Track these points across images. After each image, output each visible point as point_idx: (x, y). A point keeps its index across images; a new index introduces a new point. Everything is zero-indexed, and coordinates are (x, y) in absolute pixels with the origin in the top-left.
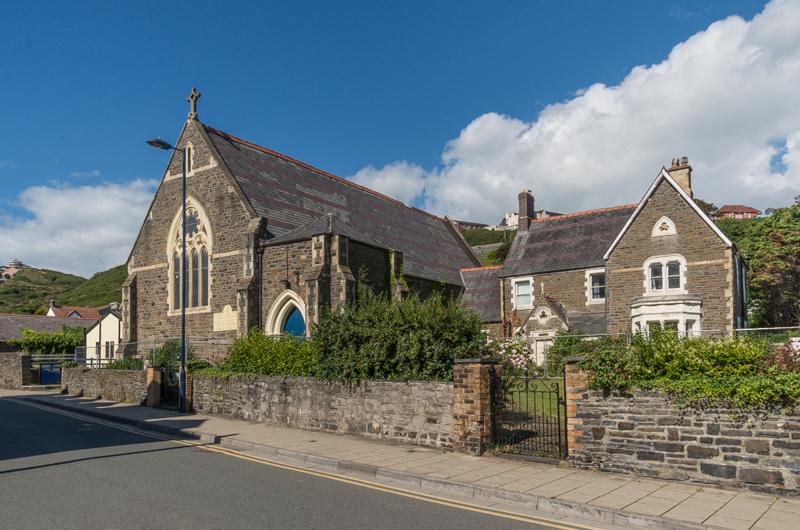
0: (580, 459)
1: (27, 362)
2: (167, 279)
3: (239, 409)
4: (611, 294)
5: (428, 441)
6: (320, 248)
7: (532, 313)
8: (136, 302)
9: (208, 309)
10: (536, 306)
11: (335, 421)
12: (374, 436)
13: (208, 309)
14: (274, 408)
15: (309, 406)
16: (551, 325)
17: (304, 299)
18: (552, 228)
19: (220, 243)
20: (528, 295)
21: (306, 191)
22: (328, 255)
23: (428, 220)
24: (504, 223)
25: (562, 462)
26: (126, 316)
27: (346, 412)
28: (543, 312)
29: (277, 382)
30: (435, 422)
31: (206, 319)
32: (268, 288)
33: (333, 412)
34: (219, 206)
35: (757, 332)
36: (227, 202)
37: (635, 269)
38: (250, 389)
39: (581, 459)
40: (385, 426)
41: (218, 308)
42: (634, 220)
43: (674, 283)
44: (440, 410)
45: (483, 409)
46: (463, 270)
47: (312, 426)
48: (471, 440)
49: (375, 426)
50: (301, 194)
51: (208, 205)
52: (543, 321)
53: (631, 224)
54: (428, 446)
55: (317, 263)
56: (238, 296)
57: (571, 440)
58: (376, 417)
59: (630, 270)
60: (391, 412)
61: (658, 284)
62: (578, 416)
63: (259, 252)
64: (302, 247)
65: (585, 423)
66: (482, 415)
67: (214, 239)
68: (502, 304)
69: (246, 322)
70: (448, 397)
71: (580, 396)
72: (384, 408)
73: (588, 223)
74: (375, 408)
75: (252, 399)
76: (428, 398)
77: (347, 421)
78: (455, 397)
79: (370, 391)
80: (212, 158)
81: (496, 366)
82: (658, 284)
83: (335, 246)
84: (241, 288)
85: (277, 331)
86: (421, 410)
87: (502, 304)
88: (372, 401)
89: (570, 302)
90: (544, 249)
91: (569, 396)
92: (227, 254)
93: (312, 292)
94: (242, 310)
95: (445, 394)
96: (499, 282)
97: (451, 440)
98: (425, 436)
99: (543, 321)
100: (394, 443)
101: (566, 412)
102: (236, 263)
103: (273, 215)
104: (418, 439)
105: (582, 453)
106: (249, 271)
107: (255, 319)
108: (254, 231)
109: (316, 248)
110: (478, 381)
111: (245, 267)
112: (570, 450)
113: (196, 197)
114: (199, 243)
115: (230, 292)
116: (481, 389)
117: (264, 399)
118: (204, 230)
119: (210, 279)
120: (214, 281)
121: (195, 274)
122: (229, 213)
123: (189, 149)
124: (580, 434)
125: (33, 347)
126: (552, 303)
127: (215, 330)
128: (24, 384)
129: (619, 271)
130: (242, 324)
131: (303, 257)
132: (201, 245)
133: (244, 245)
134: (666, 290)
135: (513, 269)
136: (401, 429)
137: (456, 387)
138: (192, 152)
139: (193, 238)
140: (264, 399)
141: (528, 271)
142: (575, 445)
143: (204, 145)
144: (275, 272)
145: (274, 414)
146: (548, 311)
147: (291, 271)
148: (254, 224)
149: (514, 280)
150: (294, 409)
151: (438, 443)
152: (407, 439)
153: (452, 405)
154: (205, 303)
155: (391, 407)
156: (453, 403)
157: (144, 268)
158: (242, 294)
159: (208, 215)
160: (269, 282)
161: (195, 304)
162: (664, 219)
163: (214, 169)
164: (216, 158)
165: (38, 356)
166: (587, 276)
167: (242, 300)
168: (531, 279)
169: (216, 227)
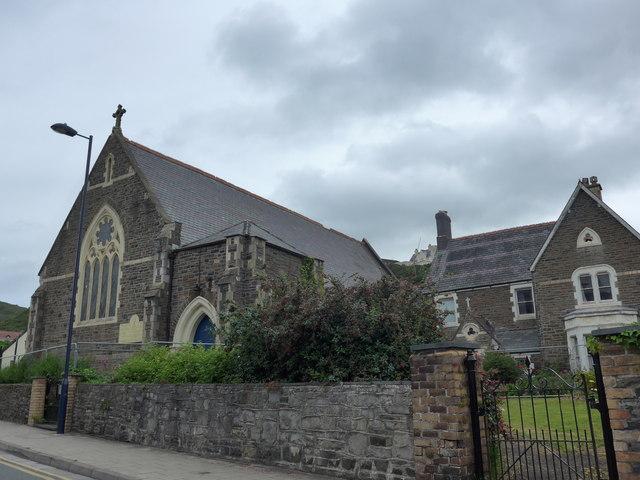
3: (123, 428)
6: (235, 250)
7: (459, 330)
10: (461, 322)
13: (115, 320)
15: (205, 422)
17: (215, 306)
18: (469, 247)
19: (132, 250)
26: (32, 327)
27: (253, 430)
28: (471, 329)
30: (382, 443)
31: (112, 330)
37: (564, 281)
41: (125, 318)
43: (606, 295)
44: (390, 424)
49: (294, 450)
51: (124, 213)
58: (294, 437)
59: (558, 281)
60: (316, 430)
61: (589, 296)
67: (126, 247)
72: (306, 424)
74: (294, 424)
77: (255, 445)
82: (589, 296)
86: (361, 426)
90: (466, 266)
91: (610, 393)
92: (138, 261)
94: (149, 319)
102: (147, 269)
106: (159, 278)
113: (113, 206)
118: (118, 237)
119: (119, 287)
120: (123, 290)
121: (105, 276)
122: (143, 219)
130: (148, 334)
131: (217, 261)
134: (598, 302)
137: (414, 387)
138: (113, 162)
140: (152, 414)
146: (476, 328)
150: (187, 428)
152: (341, 470)
154: (112, 313)
155: (317, 422)
157: (53, 279)
159: (122, 222)
161: (102, 314)
162: (587, 230)
166: (512, 291)
167: (150, 307)
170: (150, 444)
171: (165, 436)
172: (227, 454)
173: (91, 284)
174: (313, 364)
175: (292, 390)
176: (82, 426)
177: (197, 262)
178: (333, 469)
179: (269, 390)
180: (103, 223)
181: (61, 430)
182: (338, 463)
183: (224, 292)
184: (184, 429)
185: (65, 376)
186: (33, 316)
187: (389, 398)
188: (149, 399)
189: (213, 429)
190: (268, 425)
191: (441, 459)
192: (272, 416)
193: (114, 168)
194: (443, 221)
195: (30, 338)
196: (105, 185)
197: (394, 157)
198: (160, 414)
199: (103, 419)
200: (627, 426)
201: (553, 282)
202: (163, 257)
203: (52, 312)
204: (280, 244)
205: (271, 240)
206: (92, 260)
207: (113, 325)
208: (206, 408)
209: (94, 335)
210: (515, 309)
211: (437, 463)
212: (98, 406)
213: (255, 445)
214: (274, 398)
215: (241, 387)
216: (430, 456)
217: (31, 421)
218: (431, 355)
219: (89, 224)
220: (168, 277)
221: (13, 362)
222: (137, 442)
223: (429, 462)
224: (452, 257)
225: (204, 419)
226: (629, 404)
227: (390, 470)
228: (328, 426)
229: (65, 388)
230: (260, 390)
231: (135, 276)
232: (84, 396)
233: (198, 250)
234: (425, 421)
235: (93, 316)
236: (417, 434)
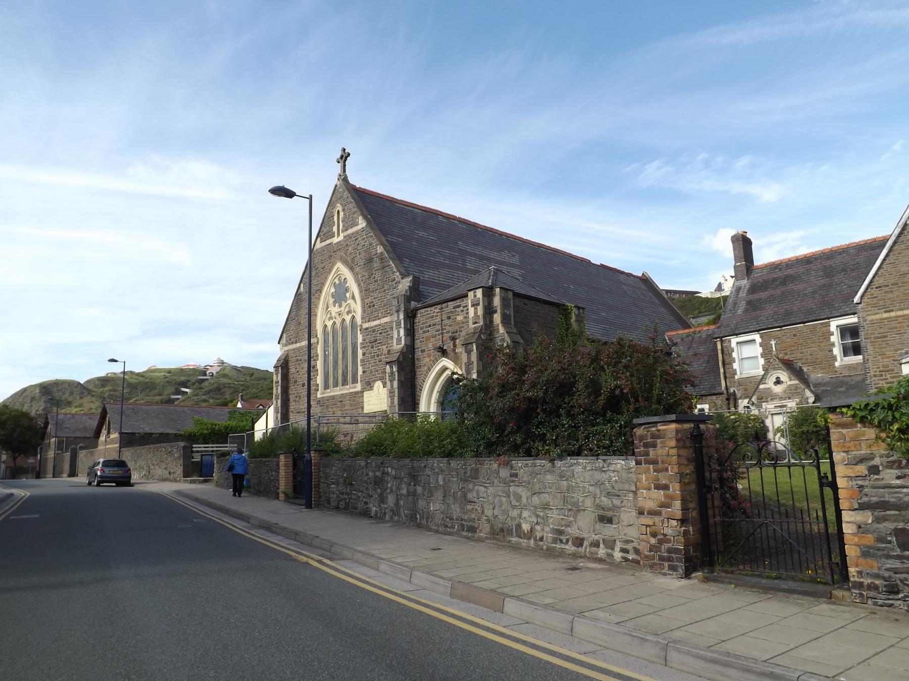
0: (873, 587)
1: (188, 453)
2: (317, 356)
3: (366, 503)
4: (870, 348)
5: (602, 552)
6: (478, 304)
7: (763, 379)
8: (288, 383)
9: (358, 387)
10: (766, 370)
11: (473, 520)
12: (524, 542)
13: (358, 387)
14: (402, 503)
16: (791, 393)
18: (778, 274)
19: (370, 310)
20: (757, 357)
22: (489, 311)
23: (622, 277)
24: (719, 288)
25: (838, 593)
26: (277, 399)
27: (486, 506)
29: (405, 466)
30: (610, 521)
31: (356, 399)
32: (423, 359)
33: (469, 507)
34: (367, 269)
36: (376, 264)
37: (900, 313)
38: (376, 477)
39: (876, 588)
40: (538, 528)
41: (369, 385)
42: (890, 250)
44: (617, 502)
45: (684, 501)
46: (669, 334)
47: (446, 526)
48: (669, 551)
49: (526, 527)
50: (466, 253)
51: (357, 269)
52: (778, 389)
53: (887, 255)
54: (601, 561)
57: (851, 551)
58: (525, 514)
59: (893, 314)
60: (546, 507)
62: (862, 507)
63: (411, 316)
64: (459, 306)
65: (877, 520)
66: (684, 509)
67: (363, 307)
68: (722, 370)
69: (396, 399)
70: (628, 481)
71: (862, 469)
72: (536, 500)
73: (827, 263)
74: (524, 500)
76: (599, 484)
77: (488, 521)
78: (638, 480)
79: (516, 475)
80: (360, 218)
81: (702, 426)
83: (497, 301)
84: (391, 360)
85: (433, 408)
86: (589, 503)
87: (722, 370)
88: (519, 490)
89: (813, 364)
90: (771, 300)
91: (840, 470)
93: (469, 358)
95: (624, 475)
96: (715, 343)
97: (637, 551)
98: (596, 544)
99: (778, 389)
100: (551, 554)
101: (837, 500)
102: (386, 330)
103: (429, 275)
104: (586, 549)
105: (877, 576)
106: (399, 340)
107: (408, 395)
109: (473, 306)
110: (674, 451)
111: (395, 336)
112: (852, 570)
113: (346, 263)
114: (348, 313)
116: (680, 465)
117: (392, 491)
118: (353, 298)
119: (360, 352)
120: (364, 354)
122: (378, 275)
124: (869, 540)
125: (192, 438)
126: (789, 365)
127: (365, 411)
129: (877, 317)
130: (392, 402)
131: (460, 318)
132: (350, 315)
133: (394, 308)
135: (733, 326)
136: (561, 532)
137: (638, 463)
138: (341, 214)
139: (342, 309)
140: (392, 491)
141: (752, 328)
142: (862, 561)
143: (352, 206)
144: (428, 339)
145: (402, 510)
146: (784, 376)
149: (734, 340)
151: (618, 555)
152: (570, 548)
153: (635, 493)
154: (355, 381)
155: (546, 498)
156: (630, 491)
157: (294, 346)
160: (423, 351)
161: (345, 382)
163: (363, 230)
164: (365, 217)
167: (392, 373)
168: (757, 337)
169: (366, 292)
170: (391, 520)
171: (404, 512)
173: (331, 350)
174: (542, 438)
175: (521, 465)
176: (329, 502)
178: (563, 546)
179: (500, 465)
181: (309, 506)
182: (567, 541)
184: (421, 503)
185: (309, 452)
186: (277, 387)
187: (616, 473)
188: (387, 473)
189: (448, 505)
190: (501, 501)
191: (665, 539)
192: (503, 492)
194: (743, 245)
195: (276, 411)
196: (335, 240)
197: (179, 493)
198: (399, 489)
199: (347, 494)
200: (856, 506)
201: (885, 315)
202: (402, 316)
203: (296, 382)
204: (533, 293)
205: (518, 290)
206: (329, 324)
207: (357, 393)
208: (441, 483)
210: (837, 351)
211: (661, 542)
212: (341, 481)
213: (488, 521)
214: (504, 473)
215: (471, 463)
216: (654, 535)
218: (654, 429)
219: (323, 284)
222: (379, 518)
223: (653, 541)
224: (753, 289)
225: (439, 495)
226: (860, 483)
227: (617, 549)
228: (556, 502)
230: (491, 465)
231: (375, 338)
232: (328, 470)
233: (439, 307)
234: (651, 498)
236: (641, 513)
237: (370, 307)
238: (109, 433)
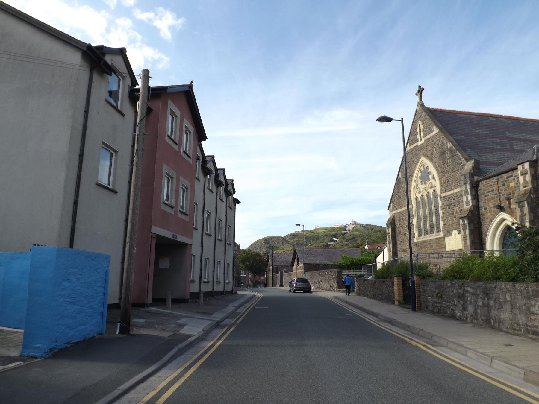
3: (453, 310)
6: (527, 173)
9: (441, 234)
13: (441, 234)
14: (479, 311)
19: (445, 185)
21: (515, 136)
26: (389, 243)
31: (441, 242)
32: (486, 214)
34: (441, 159)
35: (382, 281)
36: (448, 155)
38: (459, 293)
41: (448, 233)
51: (435, 160)
55: (525, 187)
56: (461, 221)
63: (475, 187)
64: (511, 176)
75: (461, 302)
80: (434, 127)
84: (463, 216)
85: (496, 247)
94: (465, 233)
102: (458, 197)
103: (485, 157)
106: (468, 202)
108: (468, 171)
109: (522, 175)
111: (465, 200)
113: (427, 157)
114: (431, 188)
115: (456, 221)
118: (434, 178)
119: (441, 212)
120: (443, 213)
121: (430, 212)
122: (449, 162)
123: (420, 126)
125: (341, 267)
128: (339, 289)
130: (466, 244)
131: (512, 184)
132: (432, 189)
133: (462, 182)
138: (422, 127)
139: (427, 185)
140: (471, 303)
143: (428, 120)
147: (503, 198)
148: (469, 165)
154: (438, 230)
158: (463, 221)
159: (435, 167)
160: (486, 209)
163: (437, 134)
164: (437, 126)
165: (345, 272)
167: (464, 225)
169: (441, 174)
170: (472, 322)
172: (529, 333)
173: (421, 212)
176: (427, 308)
177: (495, 187)
180: (422, 169)
181: (414, 309)
183: (522, 208)
184: (494, 313)
188: (467, 291)
193: (423, 131)
196: (419, 143)
197: (336, 298)
198: (476, 301)
199: (439, 303)
203: (400, 232)
206: (419, 196)
207: (440, 238)
209: (429, 246)
212: (435, 295)
217: (396, 302)
219: (413, 172)
220: (475, 201)
221: (383, 264)
222: (463, 320)
225: (508, 307)
229: (413, 282)
231: (451, 203)
232: (425, 288)
235: (426, 233)
237: (445, 183)
238: (298, 264)
